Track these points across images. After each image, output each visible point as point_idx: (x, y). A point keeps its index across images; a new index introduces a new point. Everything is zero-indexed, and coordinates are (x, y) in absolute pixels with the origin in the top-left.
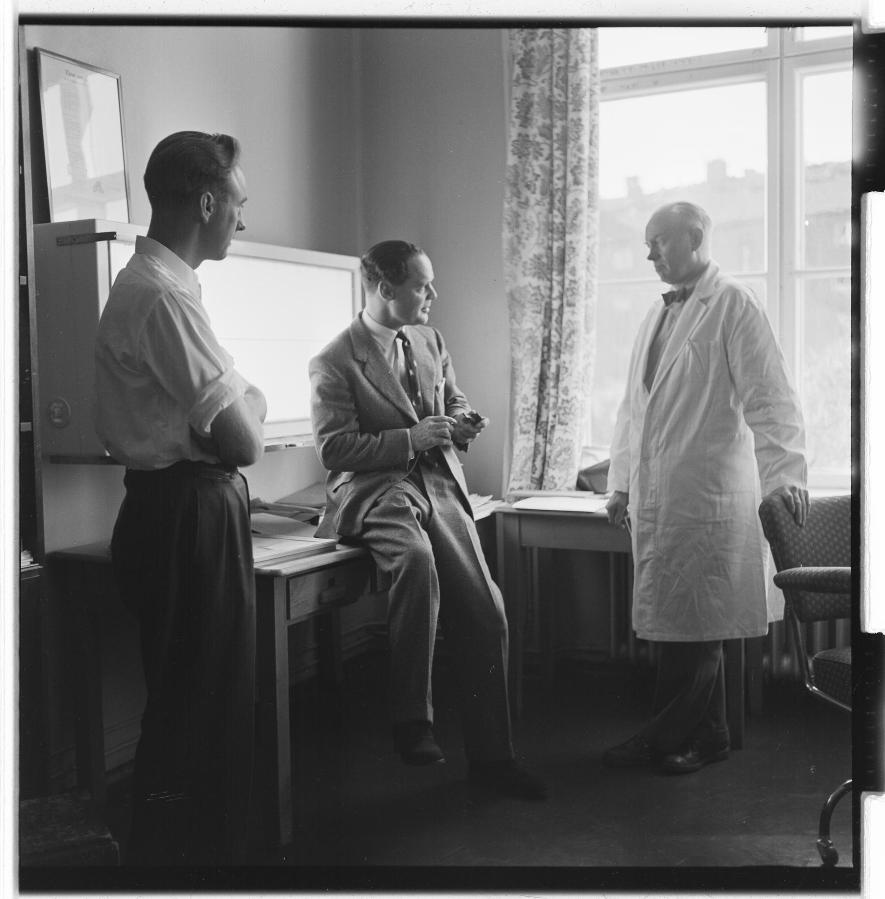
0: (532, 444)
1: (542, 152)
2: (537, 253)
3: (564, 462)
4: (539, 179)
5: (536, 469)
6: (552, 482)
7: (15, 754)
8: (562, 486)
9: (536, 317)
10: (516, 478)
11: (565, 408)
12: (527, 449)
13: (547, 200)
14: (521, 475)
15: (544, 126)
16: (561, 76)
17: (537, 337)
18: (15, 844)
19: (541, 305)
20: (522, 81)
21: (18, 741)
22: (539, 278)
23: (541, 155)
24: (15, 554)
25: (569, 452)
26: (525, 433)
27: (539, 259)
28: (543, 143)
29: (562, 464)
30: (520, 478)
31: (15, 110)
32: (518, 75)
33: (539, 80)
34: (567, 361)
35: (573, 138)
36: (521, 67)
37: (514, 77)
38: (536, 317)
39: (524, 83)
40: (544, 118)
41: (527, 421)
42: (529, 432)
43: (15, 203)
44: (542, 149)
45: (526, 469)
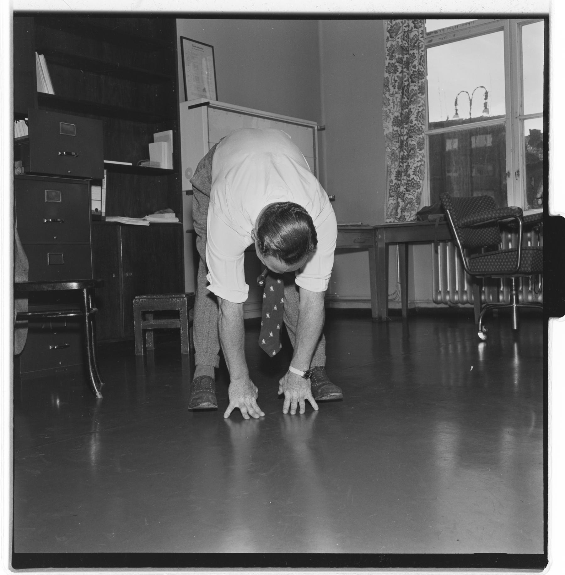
0: (395, 202)
1: (398, 70)
2: (396, 115)
3: (412, 155)
4: (397, 82)
5: (398, 214)
6: (404, 218)
7: (11, 60)
8: (412, 166)
9: (396, 144)
10: (388, 217)
11: (415, 74)
12: (393, 204)
13: (400, 92)
14: (390, 216)
15: (399, 58)
16: (405, 35)
17: (397, 153)
18: (11, 194)
19: (399, 139)
20: (390, 39)
21: (13, 65)
22: (397, 127)
23: (398, 71)
24: (11, 123)
25: (414, 150)
26: (392, 197)
27: (397, 118)
28: (398, 66)
29: (408, 209)
30: (390, 217)
31: (11, 315)
32: (388, 37)
33: (397, 38)
34: (412, 108)
35: (411, 62)
36: (389, 33)
37: (385, 38)
38: (396, 144)
39: (391, 40)
40: (399, 54)
41: (393, 191)
42: (394, 196)
43: (11, 33)
44: (398, 69)
45: (392, 213)
